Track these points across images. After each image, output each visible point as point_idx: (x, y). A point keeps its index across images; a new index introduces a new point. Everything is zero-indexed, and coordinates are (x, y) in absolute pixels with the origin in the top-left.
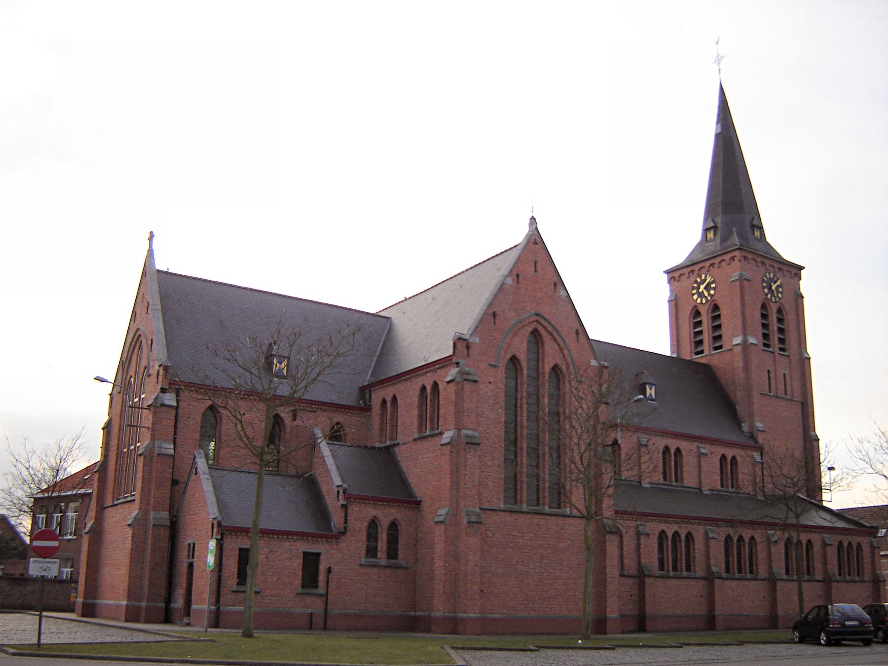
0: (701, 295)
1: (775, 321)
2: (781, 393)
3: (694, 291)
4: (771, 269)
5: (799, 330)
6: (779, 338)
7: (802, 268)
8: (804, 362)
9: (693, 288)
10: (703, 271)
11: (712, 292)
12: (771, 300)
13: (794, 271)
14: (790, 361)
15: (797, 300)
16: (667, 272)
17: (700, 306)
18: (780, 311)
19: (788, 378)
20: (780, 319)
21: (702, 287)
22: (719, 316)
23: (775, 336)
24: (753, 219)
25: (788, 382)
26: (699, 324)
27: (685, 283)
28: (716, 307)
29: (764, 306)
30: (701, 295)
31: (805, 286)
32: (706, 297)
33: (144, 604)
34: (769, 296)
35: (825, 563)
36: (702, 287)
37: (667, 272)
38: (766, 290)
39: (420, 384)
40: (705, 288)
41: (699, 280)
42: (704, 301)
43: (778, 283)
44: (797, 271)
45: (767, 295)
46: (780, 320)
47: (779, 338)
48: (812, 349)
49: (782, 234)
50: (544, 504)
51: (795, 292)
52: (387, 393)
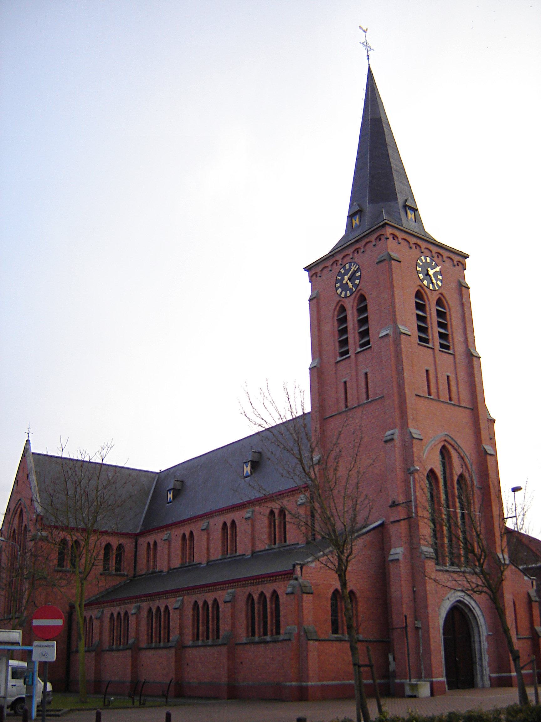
0: (345, 287)
1: (434, 314)
2: (444, 396)
3: (338, 285)
4: (428, 253)
5: (462, 305)
6: (440, 333)
7: (466, 257)
8: (472, 360)
9: (337, 281)
10: (348, 259)
11: (357, 282)
12: (428, 287)
13: (456, 258)
14: (455, 358)
15: (461, 294)
16: (307, 269)
17: (346, 300)
18: (439, 302)
19: (453, 383)
20: (444, 319)
21: (346, 277)
22: (366, 307)
23: (434, 330)
24: (406, 200)
25: (454, 389)
26: (344, 331)
27: (329, 277)
28: (363, 298)
29: (419, 295)
30: (345, 287)
31: (471, 276)
32: (351, 289)
33: (514, 674)
34: (425, 282)
35: (101, 633)
36: (346, 277)
37: (307, 269)
38: (421, 276)
39: (190, 530)
40: (349, 279)
41: (342, 271)
42: (349, 294)
43: (438, 269)
44: (461, 259)
45: (422, 281)
46: (440, 314)
47: (440, 333)
48: (481, 346)
49: (441, 208)
50: (267, 635)
51: (459, 281)
52: (151, 539)
